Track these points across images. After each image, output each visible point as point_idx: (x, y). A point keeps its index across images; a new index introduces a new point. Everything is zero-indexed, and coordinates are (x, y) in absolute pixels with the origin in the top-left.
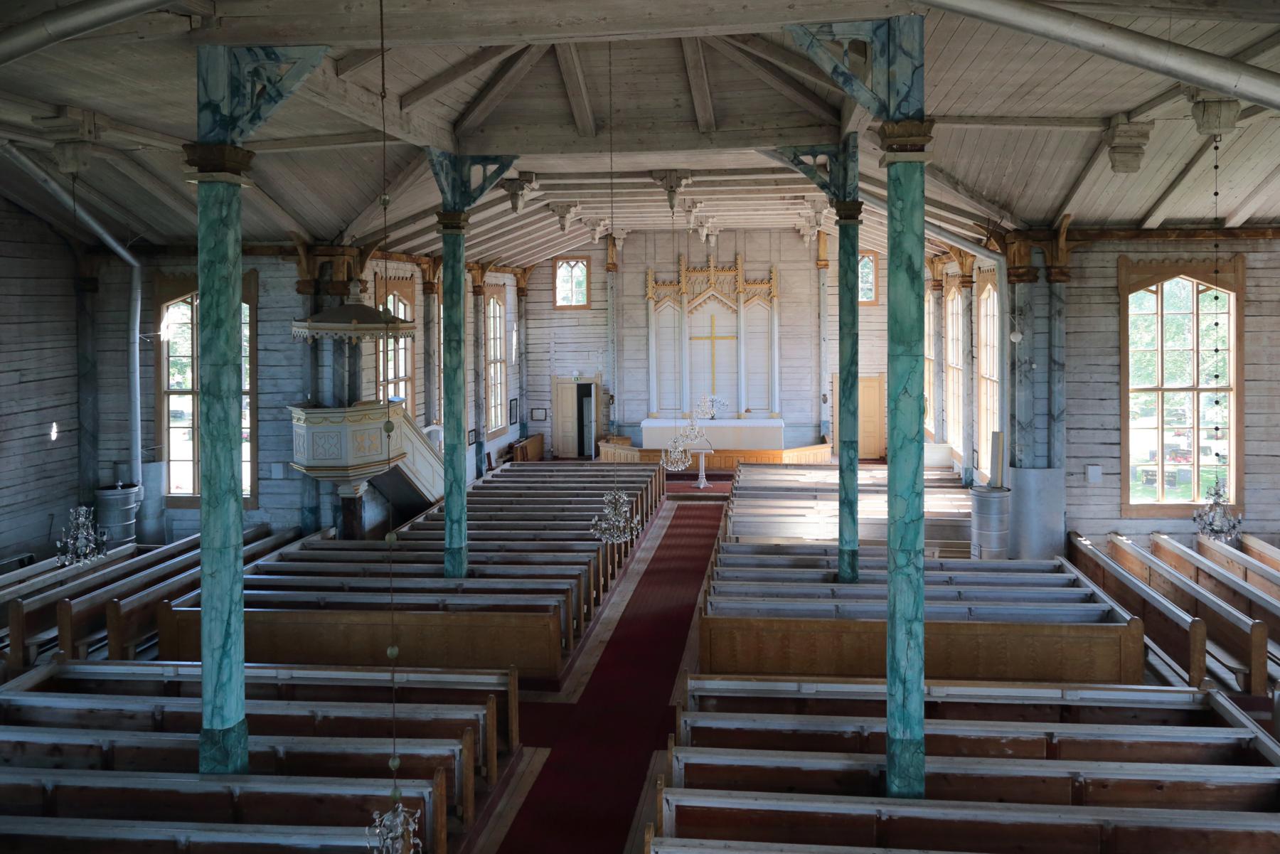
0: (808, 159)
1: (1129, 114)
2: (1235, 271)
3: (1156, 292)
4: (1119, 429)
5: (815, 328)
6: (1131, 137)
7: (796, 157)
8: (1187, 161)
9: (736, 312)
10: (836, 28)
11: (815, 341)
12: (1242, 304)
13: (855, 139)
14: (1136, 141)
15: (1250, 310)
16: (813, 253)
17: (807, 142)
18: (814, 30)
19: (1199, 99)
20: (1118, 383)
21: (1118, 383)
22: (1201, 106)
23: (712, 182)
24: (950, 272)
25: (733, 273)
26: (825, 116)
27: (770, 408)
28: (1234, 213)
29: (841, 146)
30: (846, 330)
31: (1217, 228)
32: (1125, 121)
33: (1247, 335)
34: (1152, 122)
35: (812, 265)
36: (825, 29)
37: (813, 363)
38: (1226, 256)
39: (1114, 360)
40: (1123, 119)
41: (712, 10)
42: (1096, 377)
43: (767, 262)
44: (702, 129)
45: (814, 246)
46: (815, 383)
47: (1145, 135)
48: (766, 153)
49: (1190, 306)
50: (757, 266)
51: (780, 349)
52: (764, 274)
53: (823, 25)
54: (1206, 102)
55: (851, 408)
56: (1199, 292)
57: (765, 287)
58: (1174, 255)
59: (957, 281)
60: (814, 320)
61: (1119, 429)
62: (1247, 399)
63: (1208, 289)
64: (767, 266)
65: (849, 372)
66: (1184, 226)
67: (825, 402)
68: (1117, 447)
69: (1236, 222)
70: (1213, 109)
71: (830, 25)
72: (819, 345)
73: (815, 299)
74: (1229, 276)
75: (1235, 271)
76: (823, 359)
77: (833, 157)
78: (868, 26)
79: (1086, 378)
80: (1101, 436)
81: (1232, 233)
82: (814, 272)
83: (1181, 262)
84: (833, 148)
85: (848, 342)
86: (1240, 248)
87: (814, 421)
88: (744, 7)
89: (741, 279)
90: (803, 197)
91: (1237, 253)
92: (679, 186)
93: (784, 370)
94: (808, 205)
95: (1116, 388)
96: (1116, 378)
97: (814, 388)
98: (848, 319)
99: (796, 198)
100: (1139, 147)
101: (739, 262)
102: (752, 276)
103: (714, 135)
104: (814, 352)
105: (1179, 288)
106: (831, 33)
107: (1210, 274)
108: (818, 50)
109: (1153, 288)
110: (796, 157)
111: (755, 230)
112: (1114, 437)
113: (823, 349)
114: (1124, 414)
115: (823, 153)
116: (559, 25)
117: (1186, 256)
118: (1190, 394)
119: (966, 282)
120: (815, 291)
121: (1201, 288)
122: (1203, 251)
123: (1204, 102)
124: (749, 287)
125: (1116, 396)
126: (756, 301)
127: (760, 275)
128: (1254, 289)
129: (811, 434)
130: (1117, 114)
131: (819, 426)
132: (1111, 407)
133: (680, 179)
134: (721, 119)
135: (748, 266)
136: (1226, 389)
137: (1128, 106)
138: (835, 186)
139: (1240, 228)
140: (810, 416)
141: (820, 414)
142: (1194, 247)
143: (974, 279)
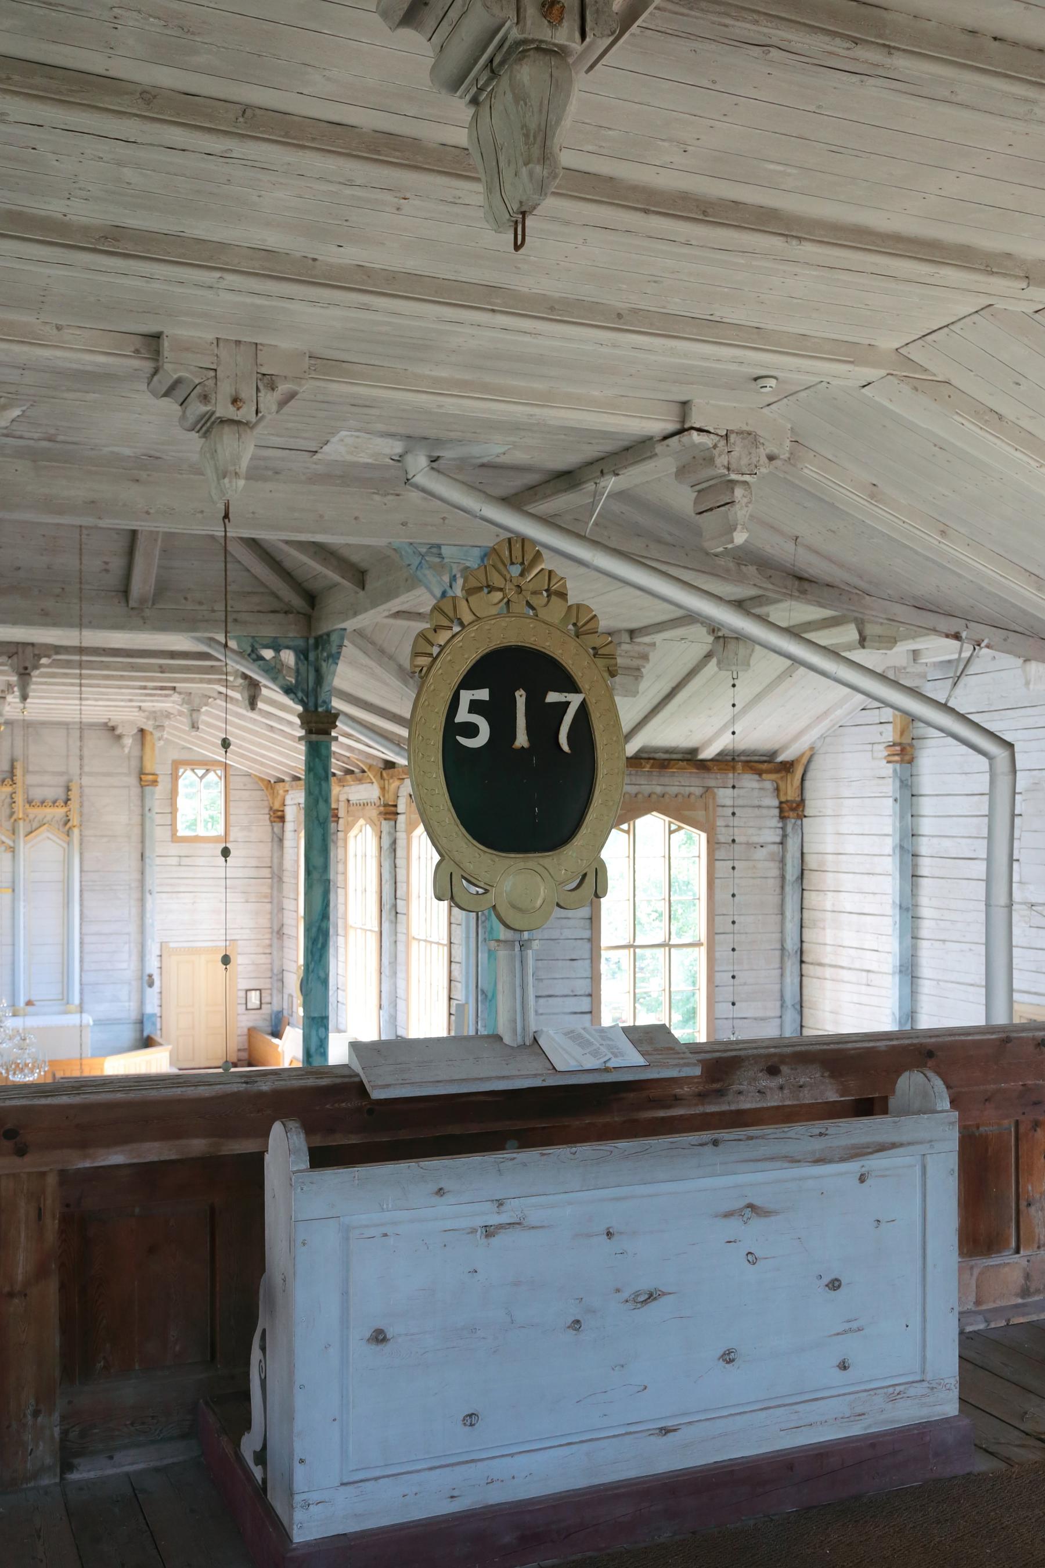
0: (268, 654)
1: (632, 633)
2: (706, 809)
3: (628, 832)
4: (590, 995)
5: (137, 876)
6: (632, 658)
7: (254, 650)
8: (673, 684)
9: (13, 850)
10: (445, 550)
11: (136, 895)
12: (713, 845)
13: (342, 638)
14: (636, 663)
15: (720, 854)
16: (135, 763)
17: (269, 631)
18: (423, 550)
19: (720, 634)
20: (590, 940)
21: (590, 940)
22: (721, 640)
23: (122, 676)
24: (353, 798)
25: (8, 789)
26: (297, 602)
27: (65, 999)
28: (709, 742)
29: (311, 641)
30: (315, 875)
31: (689, 759)
32: (628, 640)
33: (717, 881)
34: (654, 644)
35: (133, 780)
36: (434, 550)
37: (133, 928)
38: (698, 791)
39: (585, 912)
40: (626, 637)
41: (321, 516)
42: (567, 933)
43: (62, 774)
44: (132, 604)
45: (136, 753)
46: (135, 957)
47: (645, 657)
48: (198, 639)
49: (661, 849)
50: (46, 779)
51: (81, 905)
52: (60, 793)
53: (432, 546)
54: (724, 641)
55: (322, 975)
56: (671, 832)
57: (60, 812)
58: (646, 789)
59: (374, 813)
60: (134, 863)
61: (590, 995)
62: (717, 955)
63: (680, 828)
64: (62, 780)
65: (319, 929)
66: (657, 756)
67: (151, 984)
68: (588, 1016)
69: (708, 753)
70: (732, 645)
71: (439, 546)
72: (142, 901)
73: (137, 830)
74: (700, 815)
75: (706, 809)
76: (148, 921)
77: (302, 654)
78: (477, 552)
79: (555, 934)
80: (572, 1005)
81: (703, 766)
82: (135, 791)
83: (654, 797)
84: (301, 643)
85: (318, 891)
86: (711, 783)
87: (134, 1015)
88: (356, 518)
89: (20, 799)
90: (174, 688)
91: (708, 789)
92: (36, 667)
93: (87, 939)
94: (176, 697)
95: (587, 946)
96: (587, 934)
97: (134, 964)
98: (318, 861)
99: (162, 688)
100: (638, 669)
101: (19, 772)
102: (38, 794)
103: (147, 613)
104: (134, 911)
105: (651, 826)
106: (440, 555)
107: (680, 811)
108: (427, 572)
109: (625, 826)
110: (254, 650)
111: (43, 724)
112: (585, 1004)
113: (149, 905)
114: (595, 978)
115: (288, 647)
116: (148, 513)
117: (659, 789)
118: (625, 951)
119: (390, 812)
120: (136, 819)
121: (673, 827)
122: (683, 783)
123: (724, 637)
124: (33, 812)
125: (587, 955)
126: (44, 833)
127: (50, 793)
128: (723, 830)
129: (128, 1034)
130: (619, 631)
131: (141, 1022)
132: (583, 968)
133: (39, 657)
134: (162, 590)
135: (31, 779)
136: (698, 944)
137: (633, 625)
138: (303, 691)
139: (712, 760)
140: (127, 1008)
141: (142, 1003)
142: (666, 780)
143: (401, 808)
